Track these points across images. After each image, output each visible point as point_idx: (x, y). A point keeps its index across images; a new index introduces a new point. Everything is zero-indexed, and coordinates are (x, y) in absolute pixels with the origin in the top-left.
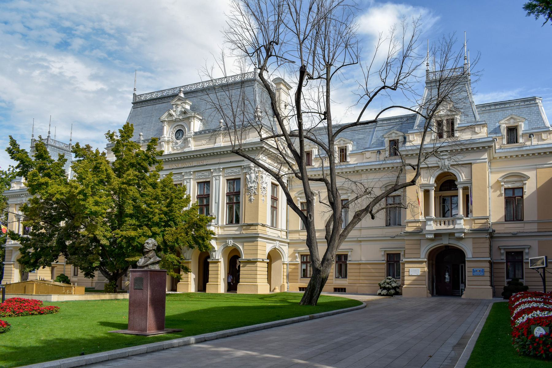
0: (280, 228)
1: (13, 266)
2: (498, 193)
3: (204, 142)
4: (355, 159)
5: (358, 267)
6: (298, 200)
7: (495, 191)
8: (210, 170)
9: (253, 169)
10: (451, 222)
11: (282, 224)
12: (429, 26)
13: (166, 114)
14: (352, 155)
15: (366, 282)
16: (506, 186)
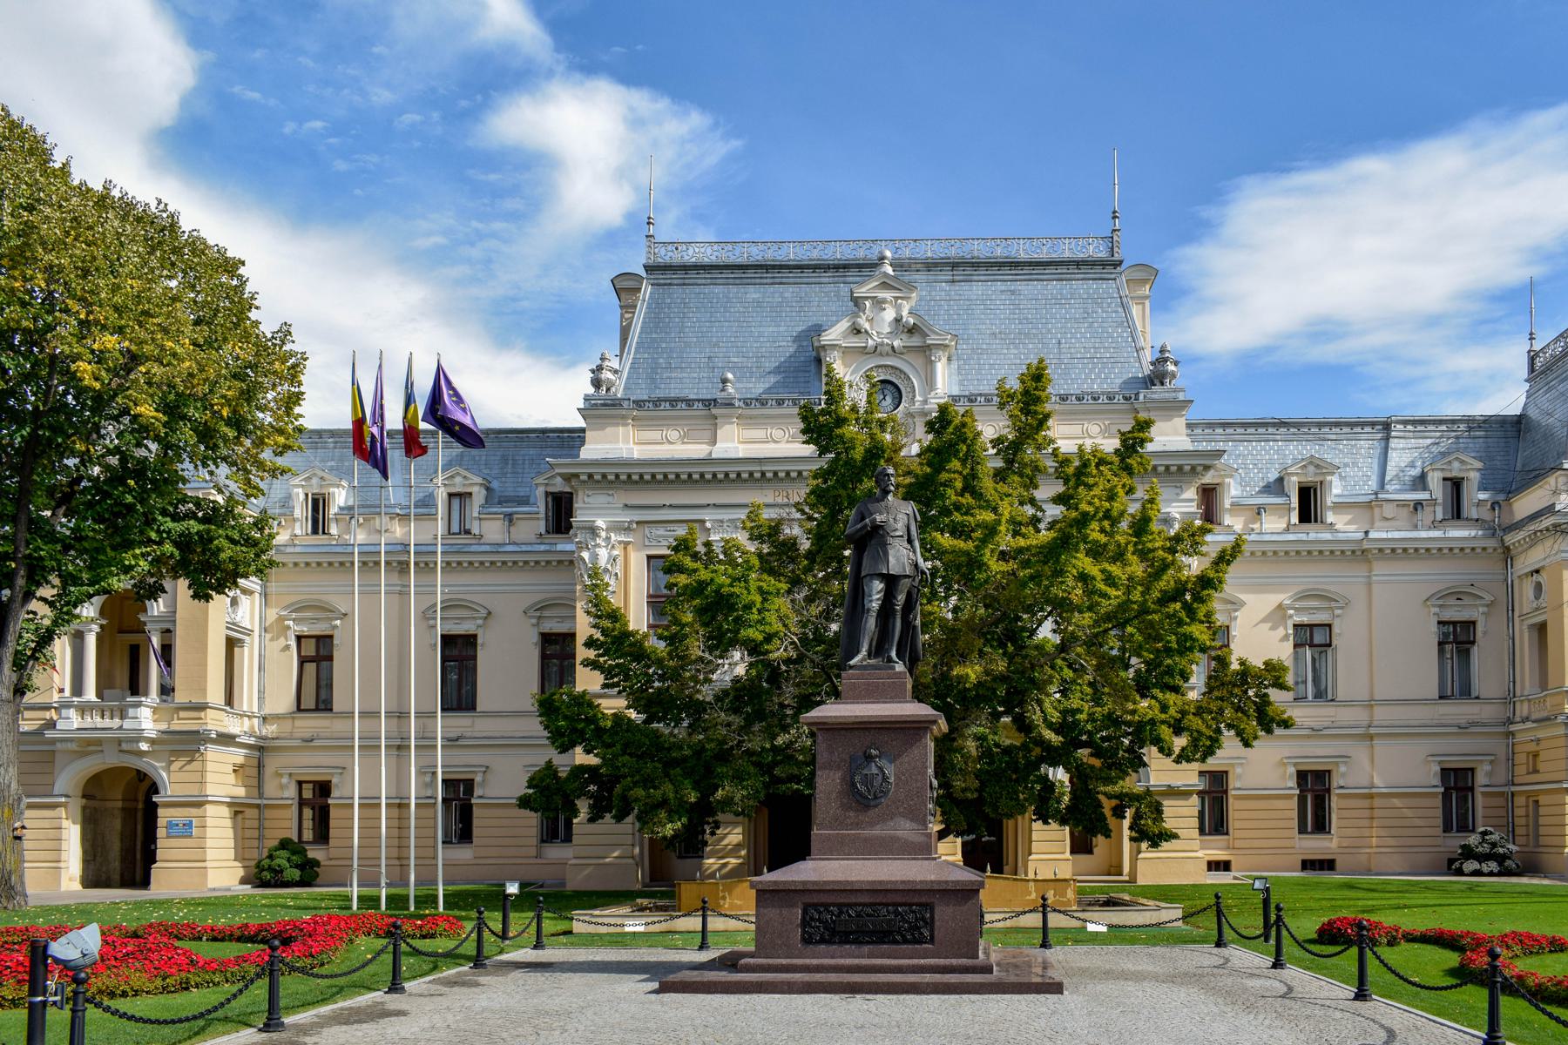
0: (1341, 696)
1: (62, 812)
2: (1281, 632)
3: (673, 435)
4: (1348, 517)
5: (1366, 803)
6: (289, 627)
7: (1273, 628)
8: (703, 522)
9: (603, 534)
10: (117, 713)
11: (248, 698)
12: (712, 160)
13: (844, 325)
14: (1339, 507)
15: (1391, 842)
16: (1298, 619)
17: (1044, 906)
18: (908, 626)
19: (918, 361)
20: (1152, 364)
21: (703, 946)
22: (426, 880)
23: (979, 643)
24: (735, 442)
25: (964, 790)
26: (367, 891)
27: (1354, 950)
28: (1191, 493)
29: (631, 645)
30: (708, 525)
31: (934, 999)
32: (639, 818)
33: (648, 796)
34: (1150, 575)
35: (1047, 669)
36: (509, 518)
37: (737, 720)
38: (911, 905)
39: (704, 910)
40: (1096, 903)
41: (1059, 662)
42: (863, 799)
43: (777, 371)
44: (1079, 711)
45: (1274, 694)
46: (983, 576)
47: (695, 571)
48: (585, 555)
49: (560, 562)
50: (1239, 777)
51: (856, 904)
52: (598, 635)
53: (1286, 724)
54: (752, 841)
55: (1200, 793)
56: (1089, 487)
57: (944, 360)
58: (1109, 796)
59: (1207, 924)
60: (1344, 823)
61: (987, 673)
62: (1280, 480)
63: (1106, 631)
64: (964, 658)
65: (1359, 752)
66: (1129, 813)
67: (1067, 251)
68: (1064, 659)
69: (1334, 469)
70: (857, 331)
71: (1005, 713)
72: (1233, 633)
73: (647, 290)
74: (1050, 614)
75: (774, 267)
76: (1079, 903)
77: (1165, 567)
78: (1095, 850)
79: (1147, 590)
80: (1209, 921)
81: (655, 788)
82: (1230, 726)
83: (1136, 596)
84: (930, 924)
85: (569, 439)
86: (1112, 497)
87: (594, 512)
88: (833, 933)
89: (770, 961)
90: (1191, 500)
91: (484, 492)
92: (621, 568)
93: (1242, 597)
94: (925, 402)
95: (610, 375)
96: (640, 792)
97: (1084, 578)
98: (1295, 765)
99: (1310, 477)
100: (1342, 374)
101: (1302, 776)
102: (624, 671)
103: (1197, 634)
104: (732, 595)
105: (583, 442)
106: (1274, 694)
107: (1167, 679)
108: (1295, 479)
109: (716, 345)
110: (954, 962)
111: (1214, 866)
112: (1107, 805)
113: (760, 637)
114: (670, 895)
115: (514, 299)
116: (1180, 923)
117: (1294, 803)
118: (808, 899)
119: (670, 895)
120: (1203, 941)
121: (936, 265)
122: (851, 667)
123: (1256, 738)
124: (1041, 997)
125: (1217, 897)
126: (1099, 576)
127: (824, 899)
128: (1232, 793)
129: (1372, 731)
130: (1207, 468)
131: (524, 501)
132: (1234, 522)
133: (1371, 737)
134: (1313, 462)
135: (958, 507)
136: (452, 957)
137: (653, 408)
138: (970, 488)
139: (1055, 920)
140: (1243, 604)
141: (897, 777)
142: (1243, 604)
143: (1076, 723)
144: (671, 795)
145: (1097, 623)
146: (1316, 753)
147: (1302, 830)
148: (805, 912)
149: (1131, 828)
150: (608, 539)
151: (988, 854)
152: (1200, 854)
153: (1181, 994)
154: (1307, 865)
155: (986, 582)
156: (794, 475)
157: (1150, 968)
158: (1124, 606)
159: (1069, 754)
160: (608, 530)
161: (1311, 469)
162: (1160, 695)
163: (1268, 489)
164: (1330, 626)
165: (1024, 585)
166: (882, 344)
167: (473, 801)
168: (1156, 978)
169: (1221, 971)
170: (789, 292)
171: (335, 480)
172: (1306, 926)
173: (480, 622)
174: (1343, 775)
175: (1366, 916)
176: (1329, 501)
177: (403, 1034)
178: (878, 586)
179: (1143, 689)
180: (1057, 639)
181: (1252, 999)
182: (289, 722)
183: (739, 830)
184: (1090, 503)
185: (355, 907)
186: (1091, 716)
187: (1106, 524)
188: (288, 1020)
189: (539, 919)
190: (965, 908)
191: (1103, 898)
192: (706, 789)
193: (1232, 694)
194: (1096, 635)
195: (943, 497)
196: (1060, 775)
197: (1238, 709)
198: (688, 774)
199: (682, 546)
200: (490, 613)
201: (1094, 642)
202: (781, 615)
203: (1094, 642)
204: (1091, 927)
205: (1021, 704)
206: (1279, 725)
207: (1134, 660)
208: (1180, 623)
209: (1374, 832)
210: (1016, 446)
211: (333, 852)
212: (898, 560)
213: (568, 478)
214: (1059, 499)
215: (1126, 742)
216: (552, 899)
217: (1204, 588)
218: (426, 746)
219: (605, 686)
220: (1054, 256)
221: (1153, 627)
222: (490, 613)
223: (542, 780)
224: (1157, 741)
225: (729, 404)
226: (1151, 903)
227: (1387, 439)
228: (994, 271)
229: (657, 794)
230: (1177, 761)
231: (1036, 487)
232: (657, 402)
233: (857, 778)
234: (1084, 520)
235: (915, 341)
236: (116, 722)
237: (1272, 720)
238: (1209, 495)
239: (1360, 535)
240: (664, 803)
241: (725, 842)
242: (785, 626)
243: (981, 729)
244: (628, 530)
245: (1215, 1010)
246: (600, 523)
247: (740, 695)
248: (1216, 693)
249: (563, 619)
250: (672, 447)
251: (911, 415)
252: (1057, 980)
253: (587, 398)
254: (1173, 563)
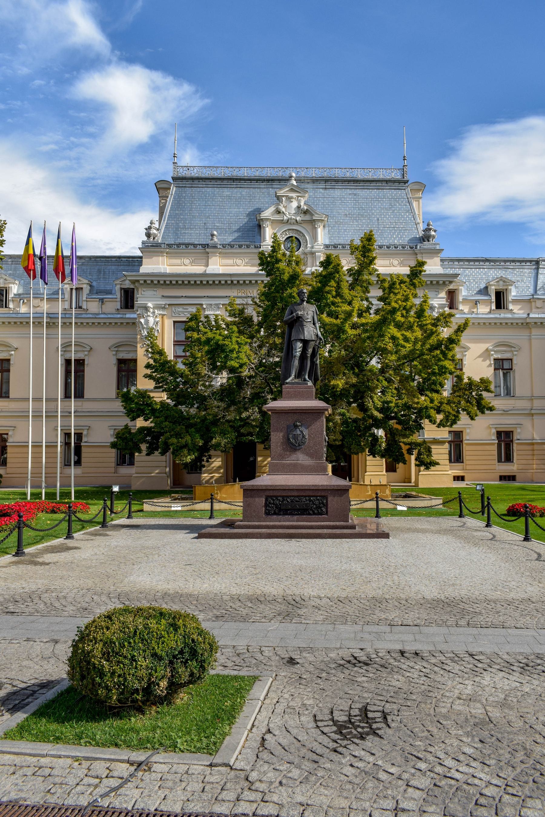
2: (488, 362)
3: (187, 261)
4: (519, 307)
5: (530, 447)
8: (202, 305)
9: (151, 310)
12: (195, 109)
13: (272, 209)
14: (515, 301)
16: (496, 356)
17: (377, 498)
18: (313, 363)
19: (309, 227)
20: (424, 231)
21: (211, 517)
22: (66, 484)
23: (343, 368)
24: (218, 266)
25: (334, 440)
26: (50, 490)
27: (523, 519)
28: (443, 294)
29: (168, 368)
30: (204, 306)
31: (329, 541)
32: (173, 453)
33: (179, 442)
34: (425, 337)
35: (375, 381)
36: (102, 301)
37: (223, 405)
38: (317, 496)
39: (212, 499)
40: (400, 496)
41: (381, 378)
42: (293, 445)
43: (238, 230)
44: (391, 402)
45: (485, 394)
46: (345, 336)
47: (206, 333)
48: (142, 321)
49: (127, 323)
50: (468, 434)
51: (291, 496)
52: (151, 362)
53: (491, 409)
54: (226, 465)
55: (449, 442)
56: (396, 294)
57: (322, 227)
58: (405, 444)
59: (454, 507)
60: (520, 457)
61: (346, 383)
62: (486, 288)
63: (404, 364)
64: (335, 375)
65: (527, 422)
66: (415, 452)
67: (381, 175)
68: (384, 376)
69: (512, 283)
70: (278, 212)
71: (354, 402)
72: (464, 363)
73: (173, 189)
74: (376, 354)
75: (237, 179)
76: (392, 497)
77: (432, 333)
78: (398, 470)
79: (423, 344)
80: (455, 506)
81: (182, 438)
82: (464, 410)
83: (418, 346)
84: (326, 506)
85: (133, 262)
86: (406, 299)
87: (146, 299)
88: (280, 510)
89: (250, 523)
90: (443, 298)
91: (89, 287)
92: (160, 325)
93: (469, 345)
94: (312, 247)
95: (155, 231)
96: (174, 440)
97: (393, 338)
98: (495, 428)
99: (501, 287)
100: (518, 228)
101: (499, 434)
102: (164, 380)
103: (447, 366)
104: (224, 345)
105: (140, 264)
106: (485, 394)
107: (433, 386)
108: (493, 287)
109: (208, 217)
110: (338, 523)
111: (458, 478)
112: (405, 448)
113: (237, 366)
114: (191, 492)
115: (93, 179)
116: (441, 506)
117: (495, 447)
118: (268, 493)
119: (191, 492)
120: (453, 514)
121: (317, 180)
122: (287, 383)
123: (476, 415)
124: (379, 540)
125: (459, 493)
126: (401, 337)
127: (276, 494)
128: (465, 442)
129: (533, 412)
130: (451, 282)
131: (109, 292)
132: (464, 308)
133: (532, 415)
134: (502, 279)
135: (333, 303)
136: (91, 522)
137: (176, 248)
138: (339, 294)
139: (383, 505)
140: (469, 348)
141: (309, 435)
142: (469, 348)
143: (389, 408)
144: (190, 442)
145: (399, 359)
146: (506, 423)
147: (499, 461)
148: (266, 500)
149: (416, 460)
150: (154, 312)
151: (344, 470)
152: (449, 472)
153: (444, 539)
154: (502, 478)
155: (346, 339)
156: (247, 282)
157: (429, 527)
158: (412, 351)
159: (385, 423)
160: (154, 308)
161: (501, 283)
162: (430, 395)
163: (480, 292)
164: (511, 360)
165: (365, 341)
166: (291, 219)
167: (82, 444)
168: (432, 532)
169: (462, 528)
170: (244, 192)
171: (13, 281)
172: (502, 508)
174: (519, 433)
175: (530, 503)
176: (510, 298)
177: (83, 557)
178: (299, 345)
179: (421, 391)
180: (379, 366)
181: (477, 541)
183: (220, 459)
184: (396, 302)
185: (29, 498)
186: (397, 405)
187: (404, 312)
188: (27, 550)
189: (130, 504)
190: (342, 498)
191: (403, 494)
192: (207, 439)
193: (464, 394)
194: (399, 366)
195: (326, 299)
196: (380, 433)
197: (468, 401)
198: (198, 431)
199: (194, 318)
200: (91, 348)
201: (397, 369)
202: (246, 356)
203: (397, 369)
204: (399, 508)
205: (362, 398)
206: (487, 410)
207: (417, 377)
208: (440, 360)
209: (535, 462)
210: (359, 273)
211: (9, 470)
212: (309, 333)
213: (133, 282)
214: (381, 299)
215: (414, 417)
216: (134, 495)
217: (451, 344)
218: (66, 415)
219: (156, 388)
220: (375, 177)
221: (426, 362)
222: (91, 348)
223: (123, 434)
224: (429, 417)
225: (215, 247)
226: (427, 496)
227: (538, 269)
228: (219, 182)
229: (183, 441)
230: (438, 426)
231: (369, 292)
232: (179, 245)
233: (291, 436)
234: (394, 311)
235: (307, 218)
237: (484, 407)
238: (452, 295)
239: (525, 316)
240: (186, 446)
241: (212, 466)
242: (249, 360)
243: (343, 410)
244: (164, 308)
245: (460, 545)
246: (150, 305)
247: (226, 393)
248: (457, 394)
249: (129, 352)
250: (186, 267)
251: (305, 254)
252: (387, 532)
253: (143, 243)
254: (436, 331)
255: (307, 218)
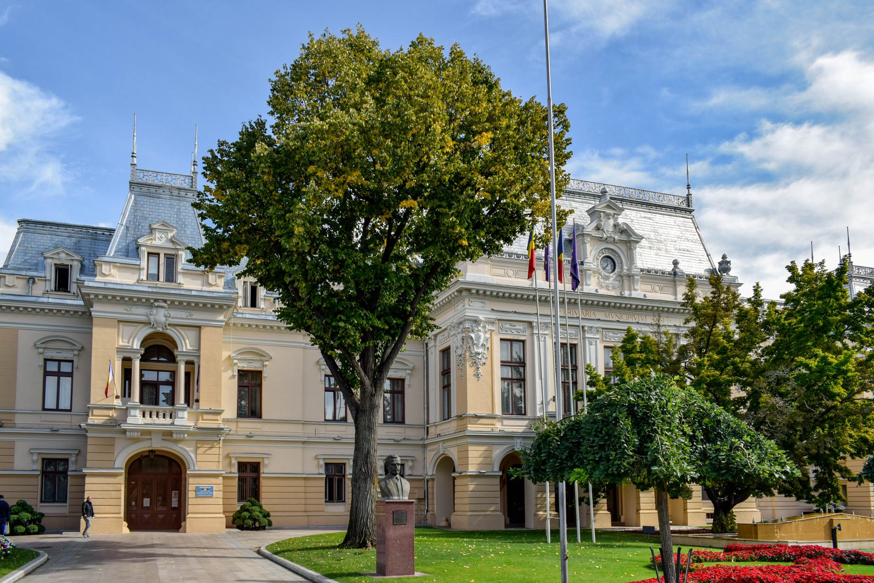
2: (230, 373)
5: (302, 483)
19: (623, 248)
117: (323, 483)
150: (484, 327)
173: (76, 352)
182: (235, 424)
222: (83, 348)
235: (624, 237)
236: (168, 421)
255: (624, 237)
